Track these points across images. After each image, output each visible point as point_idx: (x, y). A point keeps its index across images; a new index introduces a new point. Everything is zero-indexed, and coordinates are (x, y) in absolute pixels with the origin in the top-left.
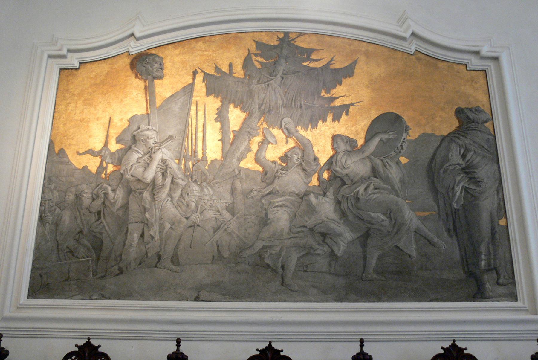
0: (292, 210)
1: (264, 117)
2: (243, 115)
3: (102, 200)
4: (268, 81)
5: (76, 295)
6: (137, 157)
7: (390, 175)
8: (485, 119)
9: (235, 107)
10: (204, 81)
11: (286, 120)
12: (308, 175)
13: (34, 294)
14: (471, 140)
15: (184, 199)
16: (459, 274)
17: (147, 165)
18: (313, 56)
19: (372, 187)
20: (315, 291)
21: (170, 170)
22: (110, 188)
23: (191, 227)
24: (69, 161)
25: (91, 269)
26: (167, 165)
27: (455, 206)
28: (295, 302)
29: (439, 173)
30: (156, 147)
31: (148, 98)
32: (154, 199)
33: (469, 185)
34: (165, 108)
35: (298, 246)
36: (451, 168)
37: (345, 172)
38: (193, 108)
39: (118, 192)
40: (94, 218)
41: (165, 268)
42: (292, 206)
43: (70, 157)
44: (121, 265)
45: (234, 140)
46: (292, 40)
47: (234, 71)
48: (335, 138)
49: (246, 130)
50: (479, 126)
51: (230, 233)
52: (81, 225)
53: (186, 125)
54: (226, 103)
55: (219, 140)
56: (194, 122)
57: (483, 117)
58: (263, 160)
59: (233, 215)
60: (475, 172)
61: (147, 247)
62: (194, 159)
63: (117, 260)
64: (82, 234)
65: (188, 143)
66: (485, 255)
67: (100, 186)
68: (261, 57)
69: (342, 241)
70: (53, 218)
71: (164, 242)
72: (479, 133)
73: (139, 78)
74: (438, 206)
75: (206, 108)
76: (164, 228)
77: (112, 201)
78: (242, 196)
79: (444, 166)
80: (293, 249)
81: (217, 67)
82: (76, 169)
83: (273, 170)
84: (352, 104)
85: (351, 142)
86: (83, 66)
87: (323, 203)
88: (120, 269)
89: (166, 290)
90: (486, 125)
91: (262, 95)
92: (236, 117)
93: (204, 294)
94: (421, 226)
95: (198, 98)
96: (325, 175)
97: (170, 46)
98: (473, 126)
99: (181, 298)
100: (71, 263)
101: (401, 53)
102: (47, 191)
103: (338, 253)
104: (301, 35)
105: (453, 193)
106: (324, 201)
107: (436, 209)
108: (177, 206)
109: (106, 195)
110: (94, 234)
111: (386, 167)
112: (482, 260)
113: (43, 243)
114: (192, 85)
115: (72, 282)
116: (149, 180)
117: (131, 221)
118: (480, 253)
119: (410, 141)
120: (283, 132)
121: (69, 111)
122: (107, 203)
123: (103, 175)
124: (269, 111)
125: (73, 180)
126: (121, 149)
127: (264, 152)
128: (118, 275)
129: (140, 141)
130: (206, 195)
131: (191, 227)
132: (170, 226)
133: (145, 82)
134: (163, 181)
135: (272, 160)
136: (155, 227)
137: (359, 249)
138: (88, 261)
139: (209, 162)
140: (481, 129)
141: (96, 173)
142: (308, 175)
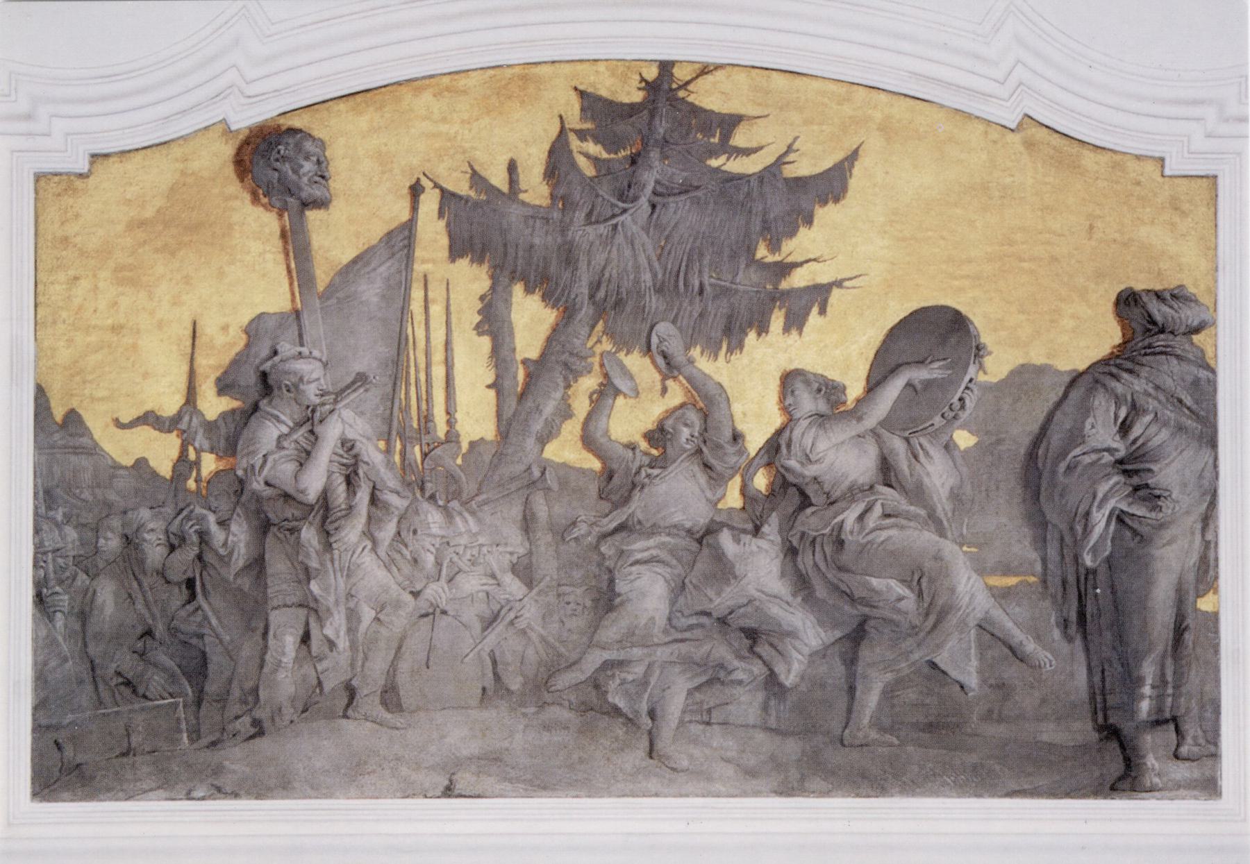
0: (676, 572)
1: (605, 322)
2: (550, 316)
3: (196, 550)
4: (614, 216)
5: (151, 790)
6: (276, 434)
7: (926, 480)
8: (1196, 323)
9: (529, 290)
10: (441, 214)
11: (663, 328)
12: (715, 477)
13: (47, 791)
14: (1148, 380)
15: (406, 546)
16: (1083, 730)
17: (304, 455)
18: (740, 139)
19: (878, 510)
20: (730, 771)
21: (365, 467)
22: (212, 518)
23: (426, 615)
24: (96, 445)
25: (183, 726)
26: (356, 456)
27: (1088, 561)
28: (681, 796)
29: (1054, 472)
30: (323, 404)
31: (293, 265)
32: (328, 547)
33: (1130, 504)
34: (340, 295)
35: (688, 663)
36: (1087, 459)
37: (811, 471)
38: (417, 294)
39: (234, 527)
40: (177, 597)
41: (366, 720)
42: (674, 562)
43: (97, 434)
44: (258, 714)
45: (527, 385)
46: (680, 87)
47: (523, 186)
48: (789, 380)
49: (558, 358)
50: (1179, 344)
51: (524, 632)
52: (147, 615)
53: (401, 343)
54: (504, 280)
55: (489, 387)
56: (420, 333)
57: (1189, 315)
58: (603, 440)
59: (530, 583)
60: (1149, 470)
61: (319, 668)
62: (426, 439)
63: (246, 703)
64: (154, 638)
65: (407, 393)
66: (1153, 687)
67: (185, 513)
68: (597, 140)
69: (795, 648)
70: (71, 598)
71: (361, 655)
72: (1174, 361)
73: (264, 206)
74: (1044, 561)
75: (452, 296)
76: (359, 621)
77: (222, 551)
78: (549, 538)
79: (1070, 456)
80: (677, 669)
81: (475, 174)
82: (117, 466)
83: (628, 469)
84: (839, 284)
85: (830, 390)
86: (100, 167)
87: (752, 553)
88: (256, 723)
89: (374, 771)
90: (1195, 338)
91: (600, 259)
92: (531, 319)
93: (464, 780)
94: (998, 614)
95: (428, 267)
96: (761, 481)
97: (342, 106)
98: (1160, 341)
99: (409, 791)
100: (130, 711)
101: (981, 127)
102: (45, 527)
103: (787, 678)
104: (705, 70)
105: (1086, 525)
106: (754, 548)
107: (1038, 567)
108: (389, 564)
109: (203, 537)
110: (182, 637)
111: (916, 457)
112: (1142, 697)
113: (53, 664)
114: (408, 230)
115: (139, 759)
116: (312, 495)
117: (275, 603)
118: (1140, 681)
119: (988, 388)
120: (654, 362)
121: (77, 301)
122: (209, 557)
123: (191, 484)
124: (619, 304)
125: (112, 496)
126: (233, 411)
127: (605, 419)
128: (252, 737)
129: (280, 388)
130: (460, 534)
131: (426, 615)
132: (373, 614)
133: (281, 216)
134: (348, 498)
135: (625, 440)
136: (336, 617)
137: (840, 669)
138: (176, 705)
139: (465, 446)
140: (1179, 352)
141: (172, 478)
142: (715, 477)
